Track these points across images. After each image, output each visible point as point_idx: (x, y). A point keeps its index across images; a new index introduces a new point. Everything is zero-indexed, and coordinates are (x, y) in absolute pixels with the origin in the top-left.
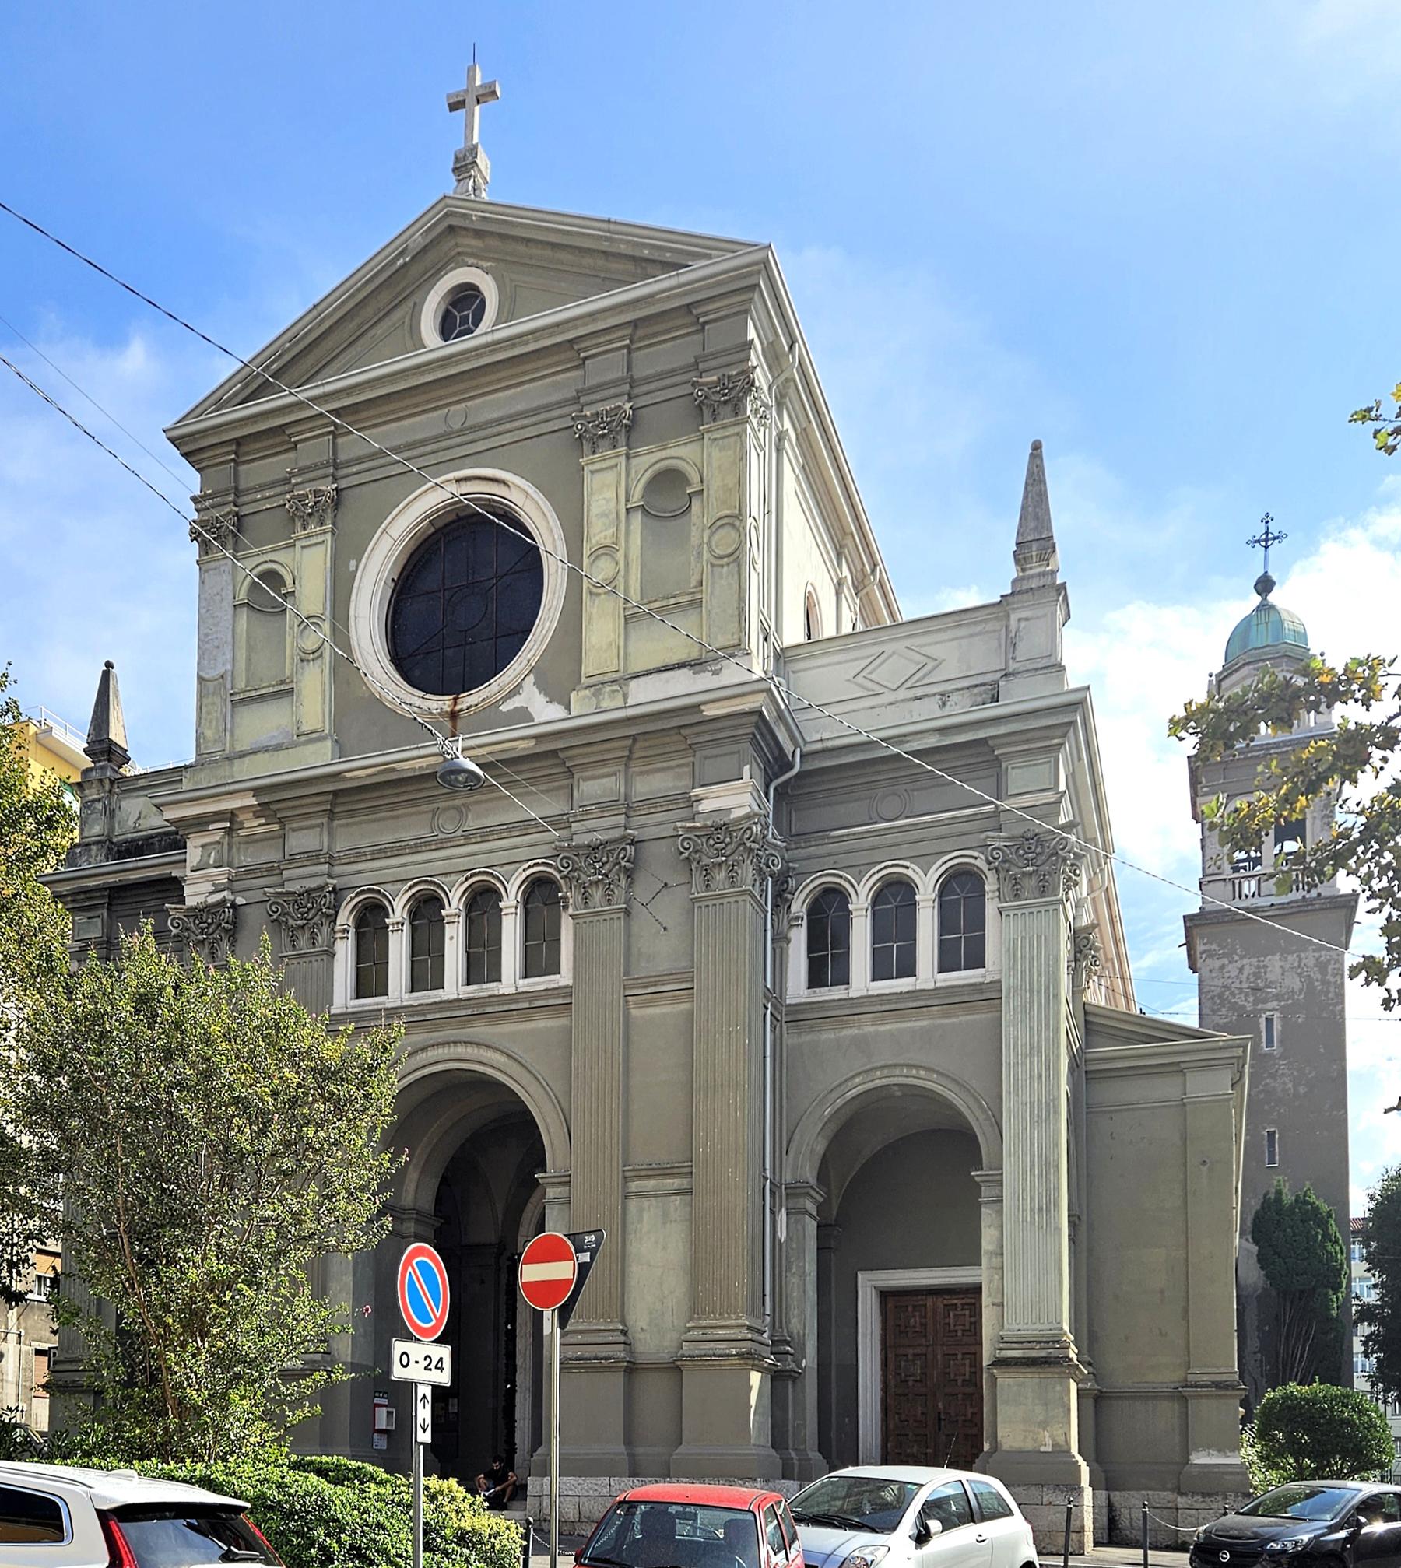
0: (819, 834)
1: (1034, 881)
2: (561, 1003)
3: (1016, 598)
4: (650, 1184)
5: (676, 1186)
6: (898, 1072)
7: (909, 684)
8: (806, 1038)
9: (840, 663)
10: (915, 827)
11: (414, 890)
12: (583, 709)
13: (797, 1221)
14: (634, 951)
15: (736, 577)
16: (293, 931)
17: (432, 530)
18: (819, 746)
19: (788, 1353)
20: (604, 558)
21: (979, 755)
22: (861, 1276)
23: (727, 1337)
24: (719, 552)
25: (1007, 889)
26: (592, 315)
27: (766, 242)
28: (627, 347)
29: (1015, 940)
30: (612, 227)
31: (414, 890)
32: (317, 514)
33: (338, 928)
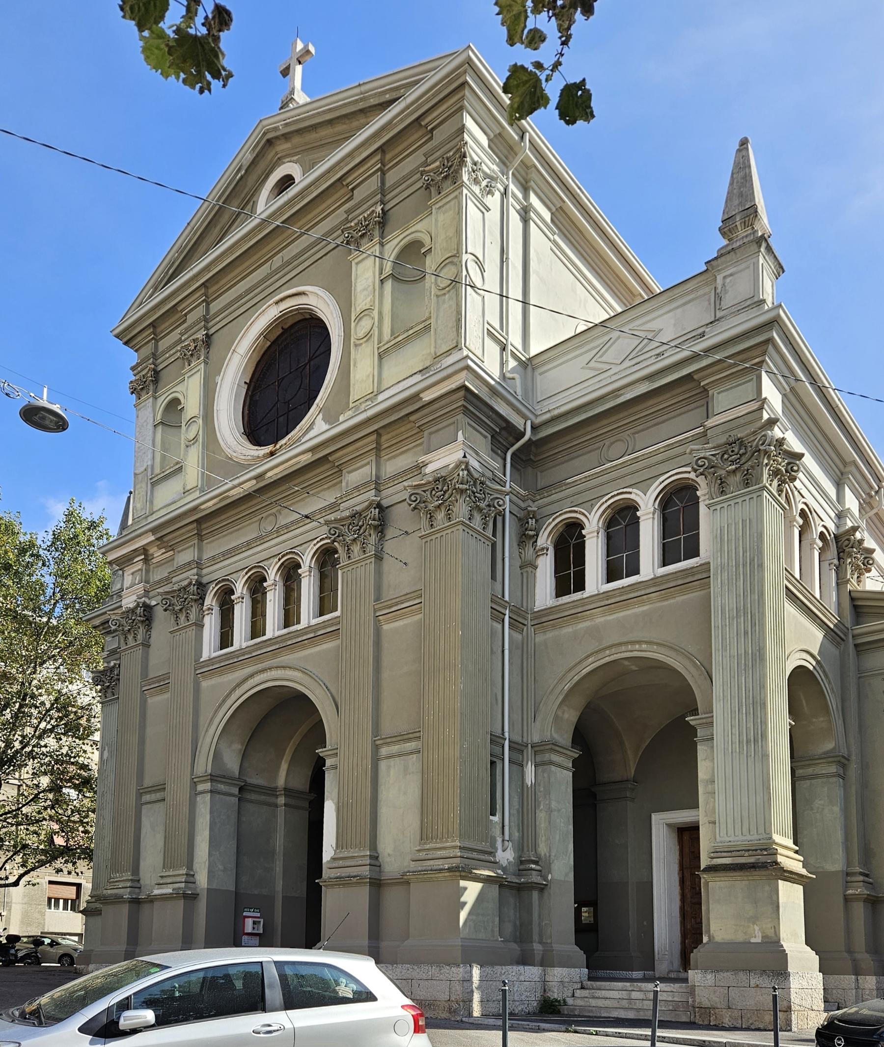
1: (738, 477)
4: (395, 749)
6: (623, 648)
7: (630, 357)
8: (550, 635)
9: (575, 357)
10: (636, 460)
13: (543, 771)
16: (176, 615)
17: (269, 343)
20: (365, 318)
21: (690, 390)
22: (655, 817)
24: (442, 286)
25: (715, 488)
26: (350, 155)
28: (379, 169)
30: (363, 88)
31: (249, 574)
33: (205, 608)
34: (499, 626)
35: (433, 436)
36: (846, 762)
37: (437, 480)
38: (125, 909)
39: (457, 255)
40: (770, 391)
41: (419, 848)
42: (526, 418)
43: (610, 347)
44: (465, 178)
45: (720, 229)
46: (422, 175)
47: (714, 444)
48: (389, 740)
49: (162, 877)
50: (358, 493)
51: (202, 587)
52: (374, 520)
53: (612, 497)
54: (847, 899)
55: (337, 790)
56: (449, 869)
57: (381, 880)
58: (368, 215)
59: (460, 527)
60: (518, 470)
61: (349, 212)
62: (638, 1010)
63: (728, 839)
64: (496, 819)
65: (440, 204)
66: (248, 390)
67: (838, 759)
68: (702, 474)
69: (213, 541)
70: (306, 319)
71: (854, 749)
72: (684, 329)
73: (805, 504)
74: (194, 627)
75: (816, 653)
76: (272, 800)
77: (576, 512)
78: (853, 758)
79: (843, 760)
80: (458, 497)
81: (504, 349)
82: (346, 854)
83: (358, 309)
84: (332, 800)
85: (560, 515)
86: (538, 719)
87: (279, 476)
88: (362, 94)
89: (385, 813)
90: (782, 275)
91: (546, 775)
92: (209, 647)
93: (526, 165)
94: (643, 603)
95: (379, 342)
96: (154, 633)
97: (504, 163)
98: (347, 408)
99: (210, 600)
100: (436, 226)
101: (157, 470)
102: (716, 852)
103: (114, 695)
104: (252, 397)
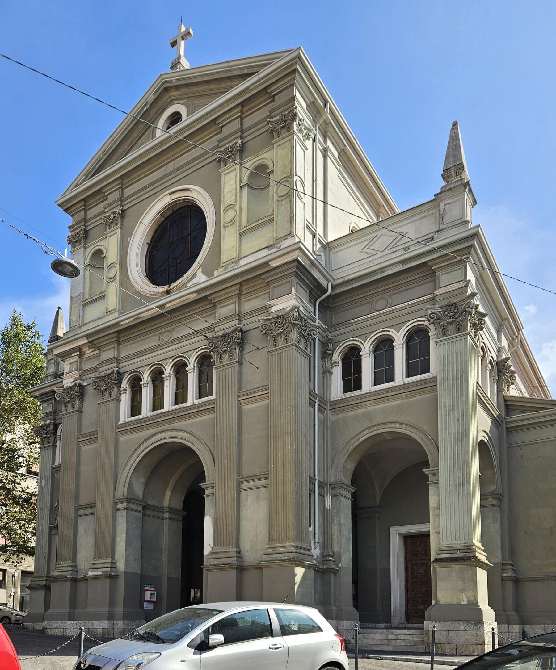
0: (345, 323)
1: (453, 326)
2: (211, 409)
3: (442, 194)
4: (251, 484)
5: (263, 484)
6: (385, 426)
8: (340, 416)
9: (355, 245)
11: (152, 369)
12: (219, 275)
13: (336, 500)
14: (244, 380)
15: (289, 203)
16: (103, 393)
17: (163, 219)
18: (341, 280)
19: (330, 560)
20: (230, 210)
22: (391, 529)
23: (284, 551)
24: (281, 195)
25: (440, 332)
27: (298, 47)
29: (444, 357)
30: (230, 64)
31: (152, 369)
32: (114, 221)
33: (122, 389)
34: (312, 410)
35: (275, 289)
36: (502, 498)
37: (279, 317)
38: (68, 585)
39: (290, 176)
40: (470, 276)
41: (268, 546)
42: (328, 281)
43: (377, 240)
44: (295, 128)
45: (442, 175)
46: (268, 124)
47: (440, 305)
48: (247, 479)
49: (93, 564)
50: (227, 322)
51: (120, 375)
52: (238, 339)
53: (378, 333)
54: (503, 579)
55: (213, 509)
56: (288, 559)
57: (243, 566)
58: (233, 145)
59: (294, 347)
60: (322, 312)
61: (220, 141)
62: (394, 646)
63: (448, 543)
64: (311, 529)
65: (279, 143)
66: (148, 248)
67: (498, 496)
68: (432, 323)
69: (127, 345)
70: (188, 206)
71: (506, 490)
72: (420, 234)
73: (484, 343)
74: (115, 401)
75: (488, 432)
76: (161, 515)
77: (356, 341)
78: (506, 495)
79: (501, 497)
80: (292, 328)
81: (314, 236)
82: (220, 550)
83: (226, 204)
84: (210, 516)
85: (347, 342)
86: (333, 469)
87: (175, 307)
88: (229, 67)
89: (245, 524)
90: (476, 206)
91: (337, 503)
92: (124, 415)
93: (327, 123)
94: (397, 399)
95: (240, 227)
96: (86, 404)
97: (314, 121)
98: (218, 266)
99: (125, 384)
100: (277, 157)
101: (87, 296)
102: (441, 550)
103: (49, 443)
104: (151, 253)
